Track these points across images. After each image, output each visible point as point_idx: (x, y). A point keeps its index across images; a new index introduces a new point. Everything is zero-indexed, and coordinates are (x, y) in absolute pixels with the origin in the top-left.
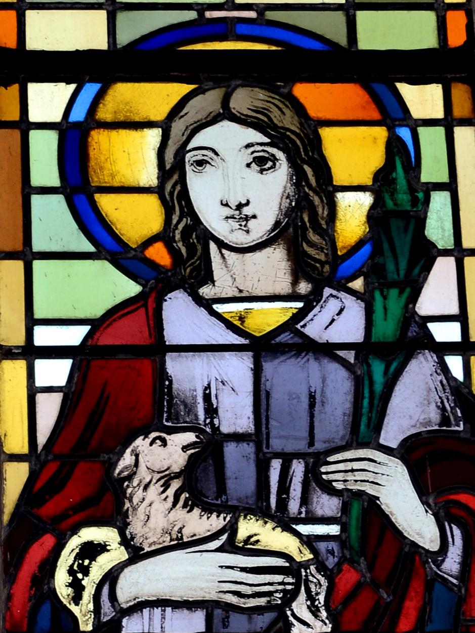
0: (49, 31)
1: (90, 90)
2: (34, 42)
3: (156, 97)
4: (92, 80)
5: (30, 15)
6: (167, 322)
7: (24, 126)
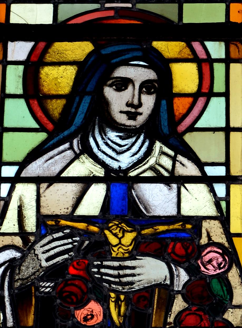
0: (22, 14)
1: (42, 45)
2: (14, 20)
3: (80, 49)
4: (43, 41)
5: (10, 58)
6: (67, 200)
7: (5, 63)
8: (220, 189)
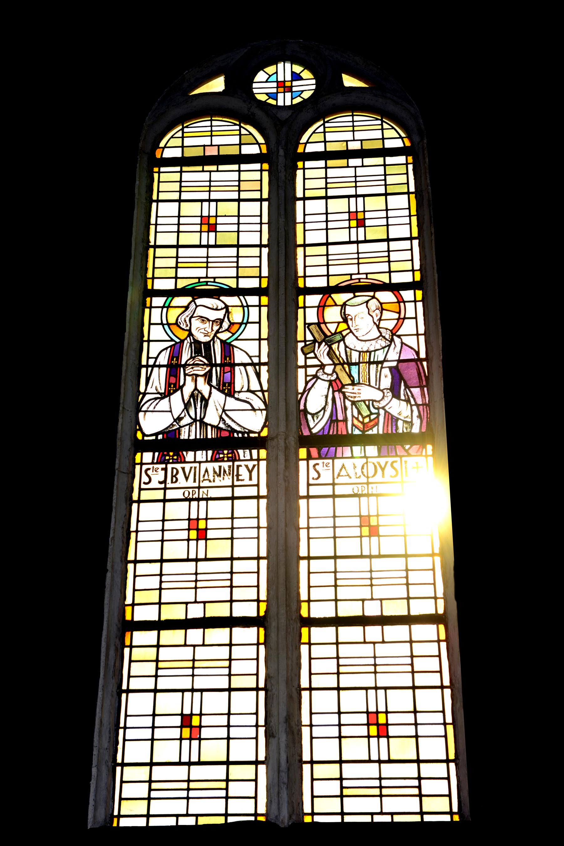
1: (170, 299)
8: (257, 367)
